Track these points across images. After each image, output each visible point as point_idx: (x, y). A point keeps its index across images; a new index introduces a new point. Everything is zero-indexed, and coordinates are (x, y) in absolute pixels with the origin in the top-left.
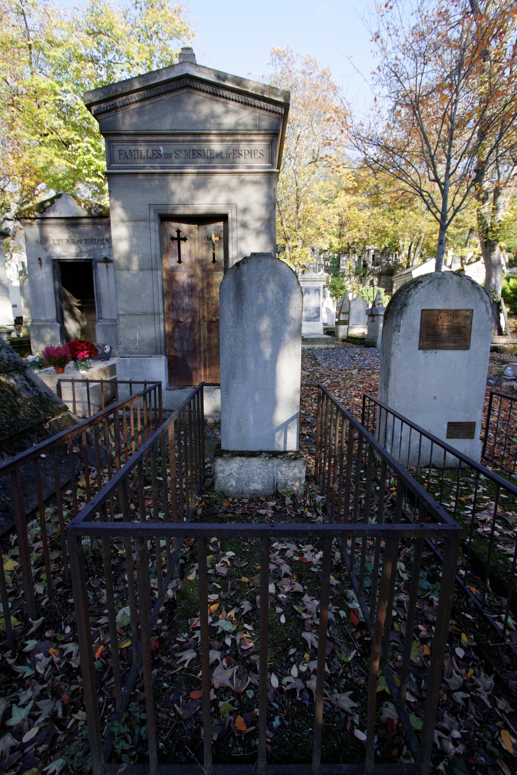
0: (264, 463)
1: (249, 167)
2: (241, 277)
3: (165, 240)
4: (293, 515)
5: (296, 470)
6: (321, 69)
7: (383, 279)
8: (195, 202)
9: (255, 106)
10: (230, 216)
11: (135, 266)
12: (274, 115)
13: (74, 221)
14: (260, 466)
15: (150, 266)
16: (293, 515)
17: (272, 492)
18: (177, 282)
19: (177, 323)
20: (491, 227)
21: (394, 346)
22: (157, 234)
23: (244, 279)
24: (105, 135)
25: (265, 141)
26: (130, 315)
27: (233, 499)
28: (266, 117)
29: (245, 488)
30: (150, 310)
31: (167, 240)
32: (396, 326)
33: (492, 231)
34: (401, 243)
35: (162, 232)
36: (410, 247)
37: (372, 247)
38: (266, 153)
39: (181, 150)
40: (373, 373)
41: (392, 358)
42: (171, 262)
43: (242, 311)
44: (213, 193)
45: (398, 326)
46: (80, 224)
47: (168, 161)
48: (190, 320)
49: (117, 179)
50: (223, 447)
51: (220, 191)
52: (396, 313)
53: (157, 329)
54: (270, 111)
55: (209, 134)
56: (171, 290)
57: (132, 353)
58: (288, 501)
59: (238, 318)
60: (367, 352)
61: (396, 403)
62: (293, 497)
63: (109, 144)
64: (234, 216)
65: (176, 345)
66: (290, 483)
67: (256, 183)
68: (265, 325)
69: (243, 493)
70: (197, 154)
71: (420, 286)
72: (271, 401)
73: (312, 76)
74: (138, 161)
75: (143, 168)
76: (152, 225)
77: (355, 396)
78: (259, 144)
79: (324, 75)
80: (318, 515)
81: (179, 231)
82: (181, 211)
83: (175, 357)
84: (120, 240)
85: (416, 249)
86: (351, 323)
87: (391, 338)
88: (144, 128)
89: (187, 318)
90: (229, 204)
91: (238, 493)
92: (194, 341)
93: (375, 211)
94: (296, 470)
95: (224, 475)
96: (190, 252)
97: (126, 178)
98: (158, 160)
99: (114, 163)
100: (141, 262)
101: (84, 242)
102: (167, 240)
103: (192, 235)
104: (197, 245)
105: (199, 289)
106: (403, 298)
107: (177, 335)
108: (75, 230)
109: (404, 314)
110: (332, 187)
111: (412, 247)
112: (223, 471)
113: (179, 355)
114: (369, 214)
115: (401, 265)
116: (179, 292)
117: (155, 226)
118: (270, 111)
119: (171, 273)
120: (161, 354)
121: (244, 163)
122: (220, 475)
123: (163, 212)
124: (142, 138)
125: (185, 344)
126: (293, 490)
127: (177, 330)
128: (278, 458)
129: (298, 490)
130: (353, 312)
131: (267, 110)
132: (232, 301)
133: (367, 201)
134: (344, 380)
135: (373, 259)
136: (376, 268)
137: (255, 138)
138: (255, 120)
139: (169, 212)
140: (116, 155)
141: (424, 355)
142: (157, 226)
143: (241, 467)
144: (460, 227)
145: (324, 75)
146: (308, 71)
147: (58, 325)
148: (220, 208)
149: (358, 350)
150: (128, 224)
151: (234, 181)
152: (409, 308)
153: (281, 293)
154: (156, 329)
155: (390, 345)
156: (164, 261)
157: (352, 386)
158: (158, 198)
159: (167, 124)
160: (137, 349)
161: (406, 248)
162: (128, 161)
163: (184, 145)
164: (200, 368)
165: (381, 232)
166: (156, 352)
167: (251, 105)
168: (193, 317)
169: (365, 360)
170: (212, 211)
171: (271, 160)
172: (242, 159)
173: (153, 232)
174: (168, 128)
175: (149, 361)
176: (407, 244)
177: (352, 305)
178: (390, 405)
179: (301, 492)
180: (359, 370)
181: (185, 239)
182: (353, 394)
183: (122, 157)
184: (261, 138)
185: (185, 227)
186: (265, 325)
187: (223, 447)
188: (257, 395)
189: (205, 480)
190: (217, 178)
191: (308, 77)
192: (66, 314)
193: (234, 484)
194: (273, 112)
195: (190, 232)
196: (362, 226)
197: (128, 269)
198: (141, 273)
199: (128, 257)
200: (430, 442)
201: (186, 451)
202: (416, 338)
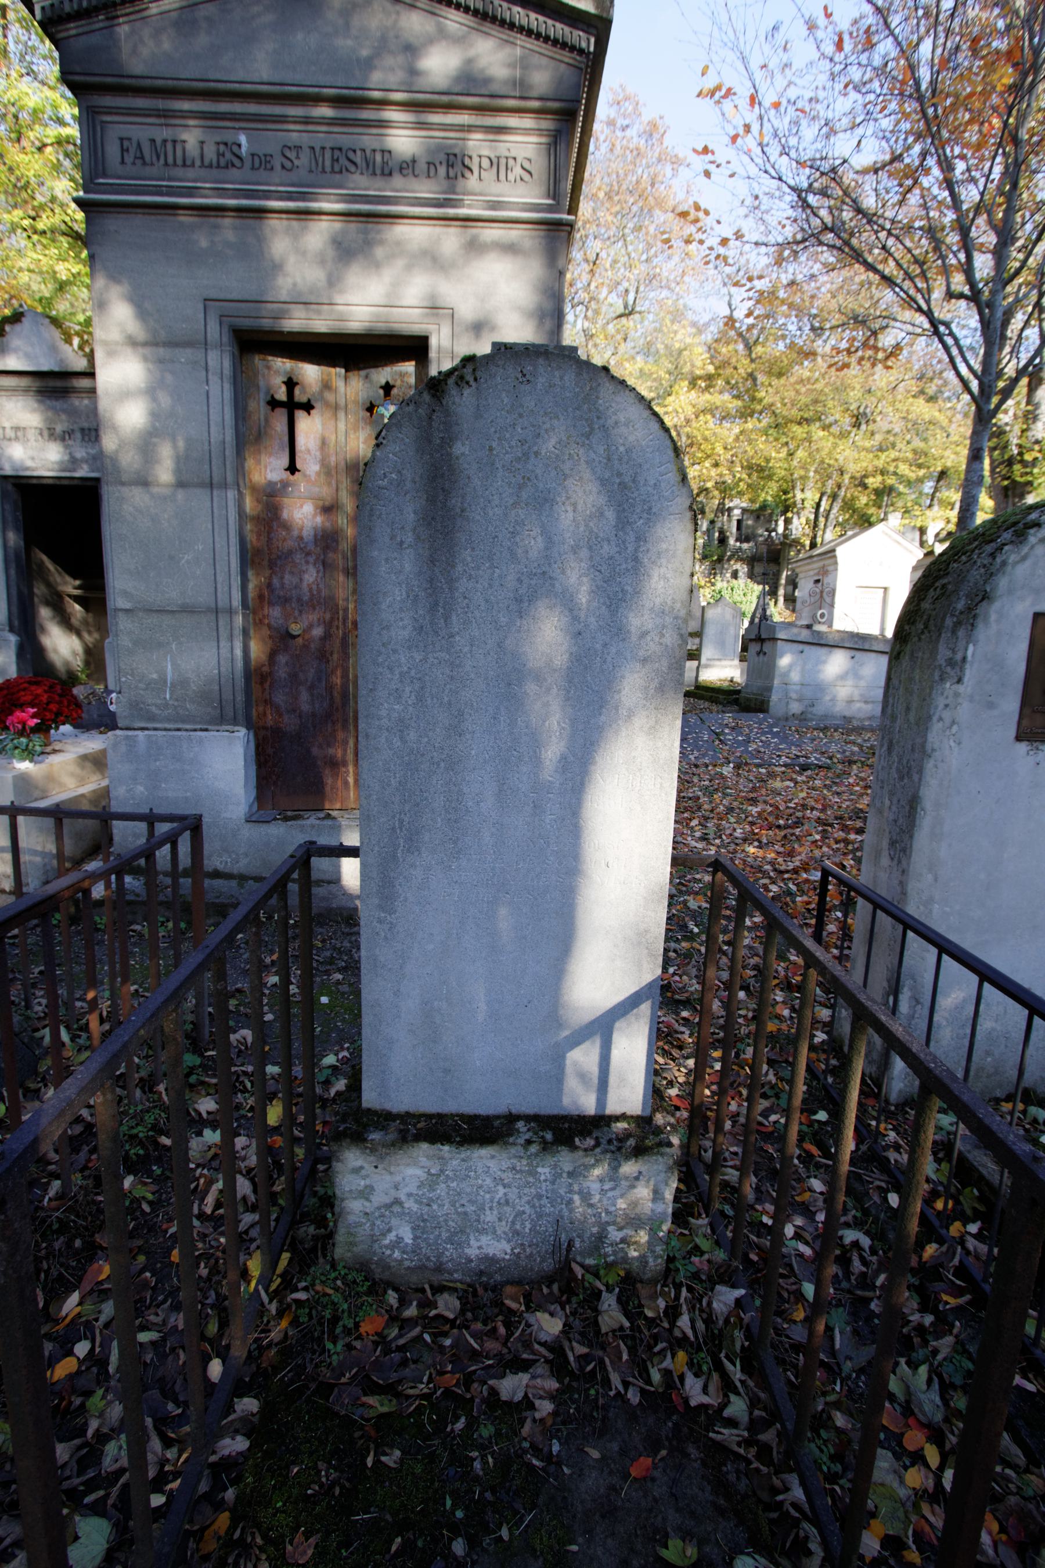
0: (523, 1164)
1: (495, 205)
2: (448, 441)
3: (252, 405)
4: (633, 1397)
5: (643, 1192)
6: (646, 117)
7: (759, 569)
8: (339, 299)
9: (512, 26)
10: (433, 342)
11: (164, 473)
12: (566, 56)
13: (58, 383)
14: (508, 1177)
15: (199, 477)
16: (633, 1397)
17: (549, 1265)
18: (287, 526)
19: (282, 640)
20: (1021, 454)
21: (936, 727)
22: (227, 386)
23: (460, 448)
24: (73, 87)
25: (539, 131)
26: (150, 611)
27: (403, 1302)
28: (544, 61)
29: (450, 1251)
30: (204, 598)
31: (258, 407)
32: (951, 663)
33: (1022, 462)
34: (799, 496)
35: (243, 385)
36: (818, 505)
37: (738, 504)
38: (539, 165)
39: (298, 148)
40: (772, 775)
41: (929, 765)
42: (269, 468)
43: (451, 582)
44: (388, 275)
45: (958, 665)
46: (75, 390)
47: (263, 174)
48: (318, 632)
49: (112, 223)
50: (370, 1098)
51: (409, 268)
52: (949, 622)
53: (225, 651)
54: (555, 42)
55: (384, 103)
56: (265, 544)
57: (152, 718)
58: (611, 1314)
59: (433, 608)
60: (751, 722)
61: (933, 901)
62: (629, 1285)
63: (89, 118)
64: (446, 343)
65: (280, 698)
66: (614, 1235)
67: (510, 249)
68: (548, 637)
69: (439, 1269)
70: (343, 161)
71: (1034, 537)
72: (555, 925)
73: (628, 133)
74: (179, 172)
75: (191, 192)
76: (214, 358)
77: (745, 840)
78: (524, 142)
79: (652, 131)
80: (728, 1386)
81: (291, 384)
82: (297, 322)
83: (277, 732)
84: (125, 395)
85: (828, 513)
86: (706, 654)
87: (926, 700)
88: (189, 72)
89: (311, 627)
90: (434, 308)
91: (422, 1268)
92: (330, 688)
93: (750, 425)
94: (643, 1192)
95: (369, 1207)
96: (324, 443)
97: (139, 219)
98: (234, 173)
99: (105, 175)
100: (181, 462)
101: (78, 435)
102: (258, 407)
103: (329, 396)
104: (342, 426)
105: (344, 546)
106: (975, 575)
107: (282, 672)
108: (58, 404)
109: (980, 626)
110: (662, 374)
111: (823, 503)
112: (366, 1193)
113: (289, 723)
114: (737, 430)
115: (796, 542)
116: (290, 552)
117: (220, 360)
118: (555, 42)
119: (271, 499)
120: (235, 722)
121: (480, 190)
122: (354, 1207)
123: (246, 323)
124: (186, 105)
125: (304, 696)
126: (625, 1259)
127: (282, 659)
128: (573, 1148)
129: (643, 1259)
130: (710, 631)
131: (547, 39)
132: (409, 538)
133: (735, 405)
134: (709, 792)
135: (739, 528)
136: (745, 546)
137: (512, 121)
138: (512, 65)
139: (266, 323)
140: (113, 151)
141: (1031, 760)
142: (227, 364)
143: (432, 1181)
144: (920, 466)
145: (652, 131)
146: (621, 122)
147: (13, 639)
148: (408, 319)
149: (728, 718)
150: (147, 351)
151: (450, 239)
152: (996, 605)
153: (610, 515)
154: (212, 657)
155: (923, 722)
156: (250, 463)
157: (730, 810)
158: (231, 282)
159: (259, 66)
160: (166, 706)
161: (809, 505)
162: (148, 171)
163: (311, 129)
164: (345, 764)
165: (760, 471)
166: (221, 718)
167: (503, 23)
168: (329, 625)
169: (748, 741)
170: (382, 327)
171: (554, 192)
172: (472, 182)
173: (214, 379)
174: (265, 77)
175: (201, 741)
176: (811, 496)
177: (710, 614)
178: (913, 909)
179: (655, 1264)
180: (737, 767)
181: (308, 407)
182: (738, 833)
183: (129, 159)
184: (527, 122)
185: (311, 373)
186: (548, 637)
187: (370, 1098)
188: (503, 911)
189: (304, 1212)
190: (402, 231)
191: (619, 133)
192: (45, 613)
193: (408, 1239)
194: (564, 45)
195: (326, 386)
196: (724, 456)
197: (144, 482)
198: (181, 495)
199: (145, 445)
200: (1018, 1014)
201: (285, 1017)
202: (1011, 704)
